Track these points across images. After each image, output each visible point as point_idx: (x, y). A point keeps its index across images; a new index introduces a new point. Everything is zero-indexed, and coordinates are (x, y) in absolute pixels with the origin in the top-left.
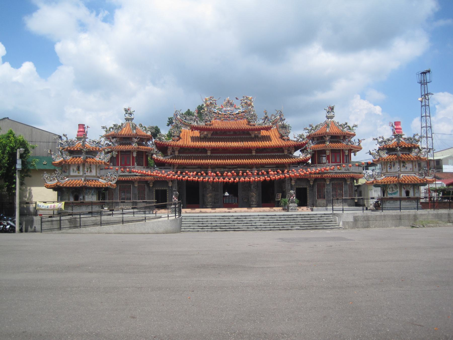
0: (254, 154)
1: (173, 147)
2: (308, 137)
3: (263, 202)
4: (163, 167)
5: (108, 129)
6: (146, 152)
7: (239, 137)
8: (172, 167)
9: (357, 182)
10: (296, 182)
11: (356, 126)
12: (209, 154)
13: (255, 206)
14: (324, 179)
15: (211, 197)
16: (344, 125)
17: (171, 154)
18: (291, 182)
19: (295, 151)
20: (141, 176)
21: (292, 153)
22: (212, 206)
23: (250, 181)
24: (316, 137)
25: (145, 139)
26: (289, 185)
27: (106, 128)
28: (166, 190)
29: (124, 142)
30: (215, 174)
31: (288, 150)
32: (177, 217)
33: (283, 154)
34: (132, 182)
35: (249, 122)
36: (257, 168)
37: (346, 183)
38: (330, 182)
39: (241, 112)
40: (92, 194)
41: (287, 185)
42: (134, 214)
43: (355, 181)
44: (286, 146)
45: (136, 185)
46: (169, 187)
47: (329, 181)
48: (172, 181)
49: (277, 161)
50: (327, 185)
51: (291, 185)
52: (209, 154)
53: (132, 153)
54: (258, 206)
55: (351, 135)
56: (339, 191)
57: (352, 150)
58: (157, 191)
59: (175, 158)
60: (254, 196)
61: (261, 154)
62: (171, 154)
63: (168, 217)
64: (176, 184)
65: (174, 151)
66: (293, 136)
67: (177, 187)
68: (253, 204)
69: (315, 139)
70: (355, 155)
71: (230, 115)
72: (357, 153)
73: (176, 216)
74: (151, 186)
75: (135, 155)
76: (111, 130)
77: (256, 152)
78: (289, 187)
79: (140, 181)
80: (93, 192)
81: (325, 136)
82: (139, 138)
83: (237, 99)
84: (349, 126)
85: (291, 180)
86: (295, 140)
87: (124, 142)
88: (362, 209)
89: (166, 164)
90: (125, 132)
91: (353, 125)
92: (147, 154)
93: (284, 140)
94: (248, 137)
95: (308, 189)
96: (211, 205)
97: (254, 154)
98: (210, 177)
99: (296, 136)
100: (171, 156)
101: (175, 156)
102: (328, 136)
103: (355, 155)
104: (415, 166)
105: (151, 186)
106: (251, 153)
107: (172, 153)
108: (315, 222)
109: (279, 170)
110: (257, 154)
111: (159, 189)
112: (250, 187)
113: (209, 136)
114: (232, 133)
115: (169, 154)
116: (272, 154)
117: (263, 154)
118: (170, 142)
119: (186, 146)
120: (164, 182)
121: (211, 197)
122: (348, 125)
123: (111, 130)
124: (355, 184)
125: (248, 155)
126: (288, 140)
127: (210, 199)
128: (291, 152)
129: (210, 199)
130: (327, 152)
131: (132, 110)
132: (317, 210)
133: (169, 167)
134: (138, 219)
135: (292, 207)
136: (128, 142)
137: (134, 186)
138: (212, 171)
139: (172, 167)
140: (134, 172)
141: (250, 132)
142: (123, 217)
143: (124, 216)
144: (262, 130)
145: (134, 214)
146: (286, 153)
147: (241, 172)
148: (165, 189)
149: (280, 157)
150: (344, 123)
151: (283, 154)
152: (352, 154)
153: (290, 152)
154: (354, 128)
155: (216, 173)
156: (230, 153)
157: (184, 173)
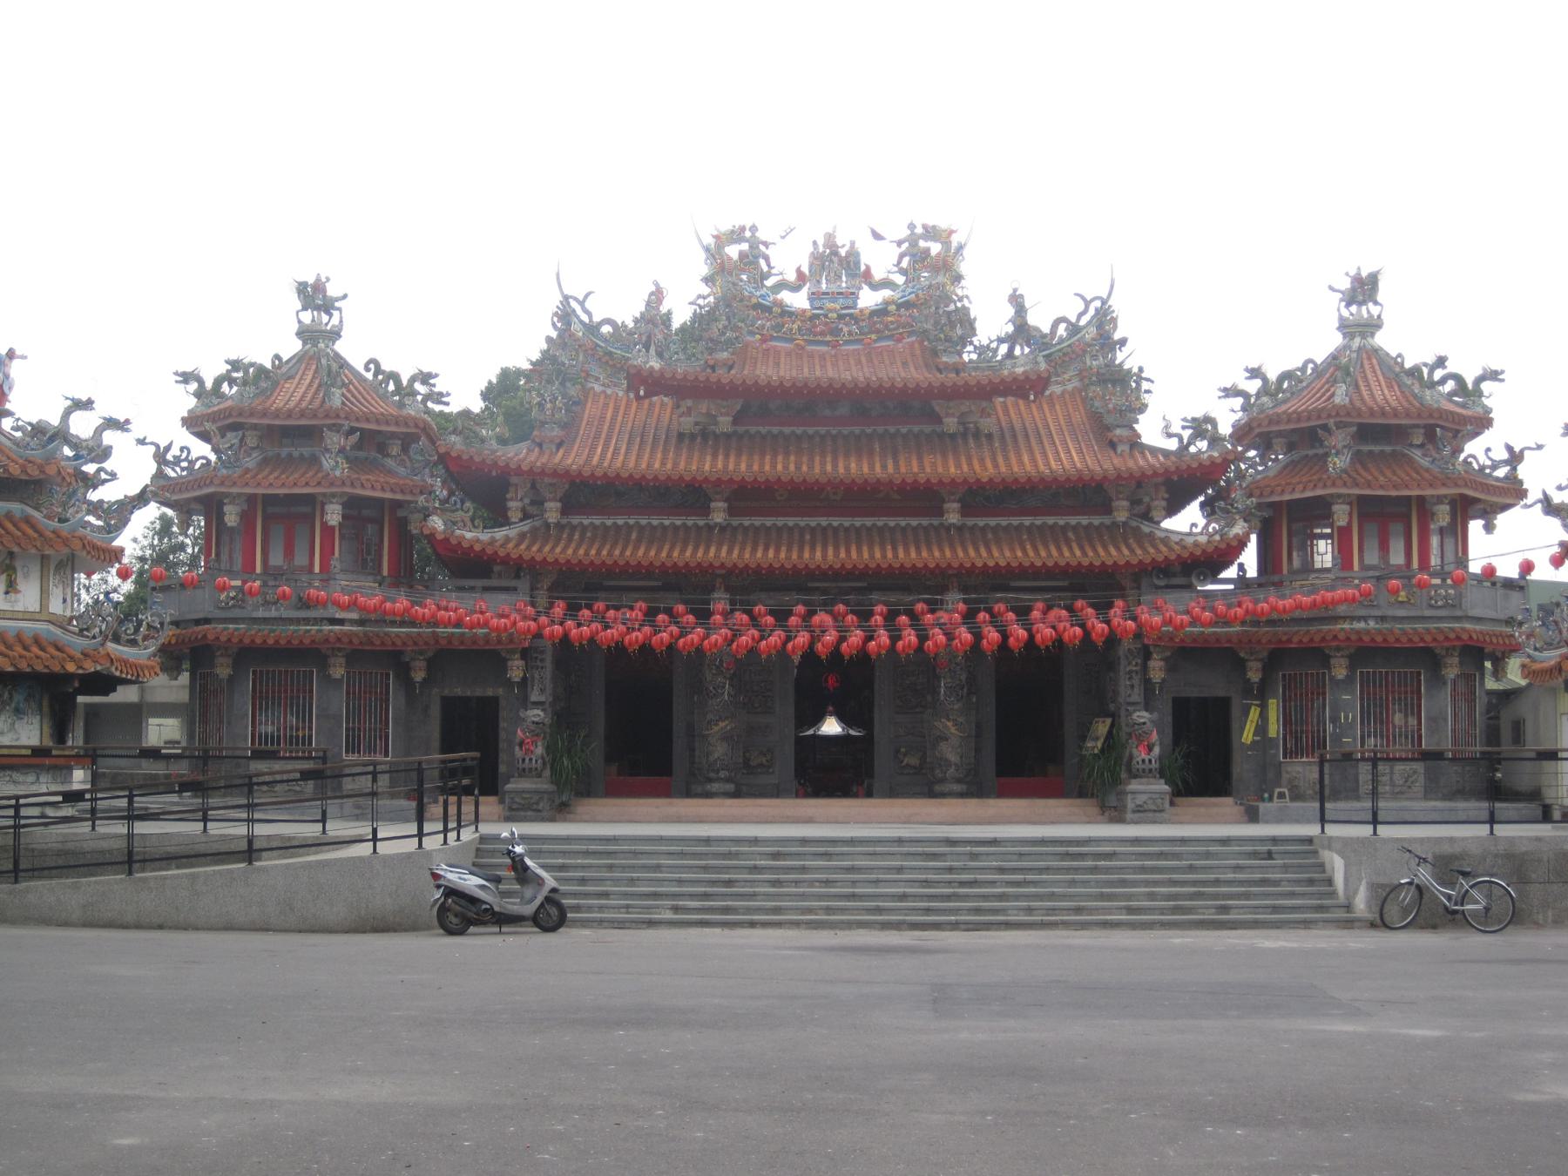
0: (953, 518)
1: (534, 478)
2: (1242, 433)
3: (1001, 772)
4: (480, 583)
5: (209, 385)
6: (397, 504)
7: (880, 429)
8: (523, 584)
9: (1498, 672)
10: (1171, 667)
11: (1493, 375)
12: (719, 517)
13: (956, 787)
14: (1318, 655)
15: (726, 737)
16: (1432, 369)
17: (526, 516)
18: (1145, 668)
19: (1173, 509)
20: (361, 622)
21: (1155, 514)
22: (731, 787)
23: (862, 657)
24: (1280, 434)
25: (393, 435)
26: (1136, 680)
27: (201, 382)
28: (495, 700)
29: (284, 452)
30: (745, 617)
31: (1135, 502)
32: (428, 843)
33: (1107, 520)
34: (311, 655)
35: (935, 353)
36: (964, 589)
37: (1437, 679)
38: (1352, 667)
39: (899, 306)
40: (18, 712)
41: (1124, 682)
42: (205, 820)
43: (1488, 664)
44: (1119, 477)
45: (338, 672)
46: (509, 683)
47: (1344, 662)
48: (525, 654)
49: (1073, 555)
50: (1336, 683)
51: (1147, 682)
52: (719, 517)
53: (323, 504)
54: (975, 787)
55: (1465, 420)
56: (1398, 718)
57: (1477, 501)
58: (449, 704)
59: (543, 533)
60: (952, 736)
61: (993, 522)
62: (526, 516)
63: (375, 839)
64: (548, 673)
65: (538, 502)
66: (1157, 428)
67: (549, 686)
68: (942, 781)
69: (1278, 443)
70: (1489, 528)
71: (841, 317)
72: (1501, 519)
73: (420, 835)
74: (419, 676)
75: (334, 515)
76: (225, 387)
77: (966, 511)
78: (1137, 696)
79: (357, 655)
80: (18, 697)
81: (1325, 427)
82: (352, 431)
83: (877, 236)
84: (1458, 379)
85: (1146, 654)
86: (1172, 445)
87: (284, 452)
88: (1485, 815)
89: (497, 568)
90: (291, 396)
91: (1479, 372)
92: (400, 513)
93: (1112, 445)
94: (927, 429)
95: (446, 692)
96: (728, 780)
97: (953, 518)
98: (723, 632)
99: (1176, 429)
100: (525, 526)
101: (548, 526)
102: (1339, 425)
103: (1489, 528)
104: (704, 437)
105: (419, 676)
106: (940, 512)
107: (532, 510)
108: (1217, 882)
109: (1079, 603)
110: (970, 522)
111: (458, 692)
112: (935, 692)
113: (725, 423)
114: (843, 410)
115: (514, 516)
116: (1050, 520)
117: (1004, 522)
118: (520, 454)
119: (599, 473)
120: (485, 657)
121: (726, 737)
122: (1451, 367)
123: (225, 387)
124: (1491, 684)
125: (925, 522)
126: (1135, 443)
127: (719, 750)
128: (1149, 509)
129: (719, 750)
130: (1335, 508)
131: (332, 291)
132: (1280, 819)
133: (513, 583)
134: (224, 848)
135: (1141, 799)
136: (306, 451)
137: (327, 679)
138: (733, 603)
139: (523, 584)
140: (322, 603)
141: (938, 406)
142: (130, 836)
143: (141, 828)
144: (1004, 394)
145: (205, 820)
146: (1121, 516)
147: (878, 608)
148: (490, 693)
149: (1088, 535)
150: (1431, 360)
151: (1107, 520)
152: (1475, 527)
153: (1140, 509)
154: (1486, 386)
155: (749, 613)
156: (832, 510)
157: (586, 613)
